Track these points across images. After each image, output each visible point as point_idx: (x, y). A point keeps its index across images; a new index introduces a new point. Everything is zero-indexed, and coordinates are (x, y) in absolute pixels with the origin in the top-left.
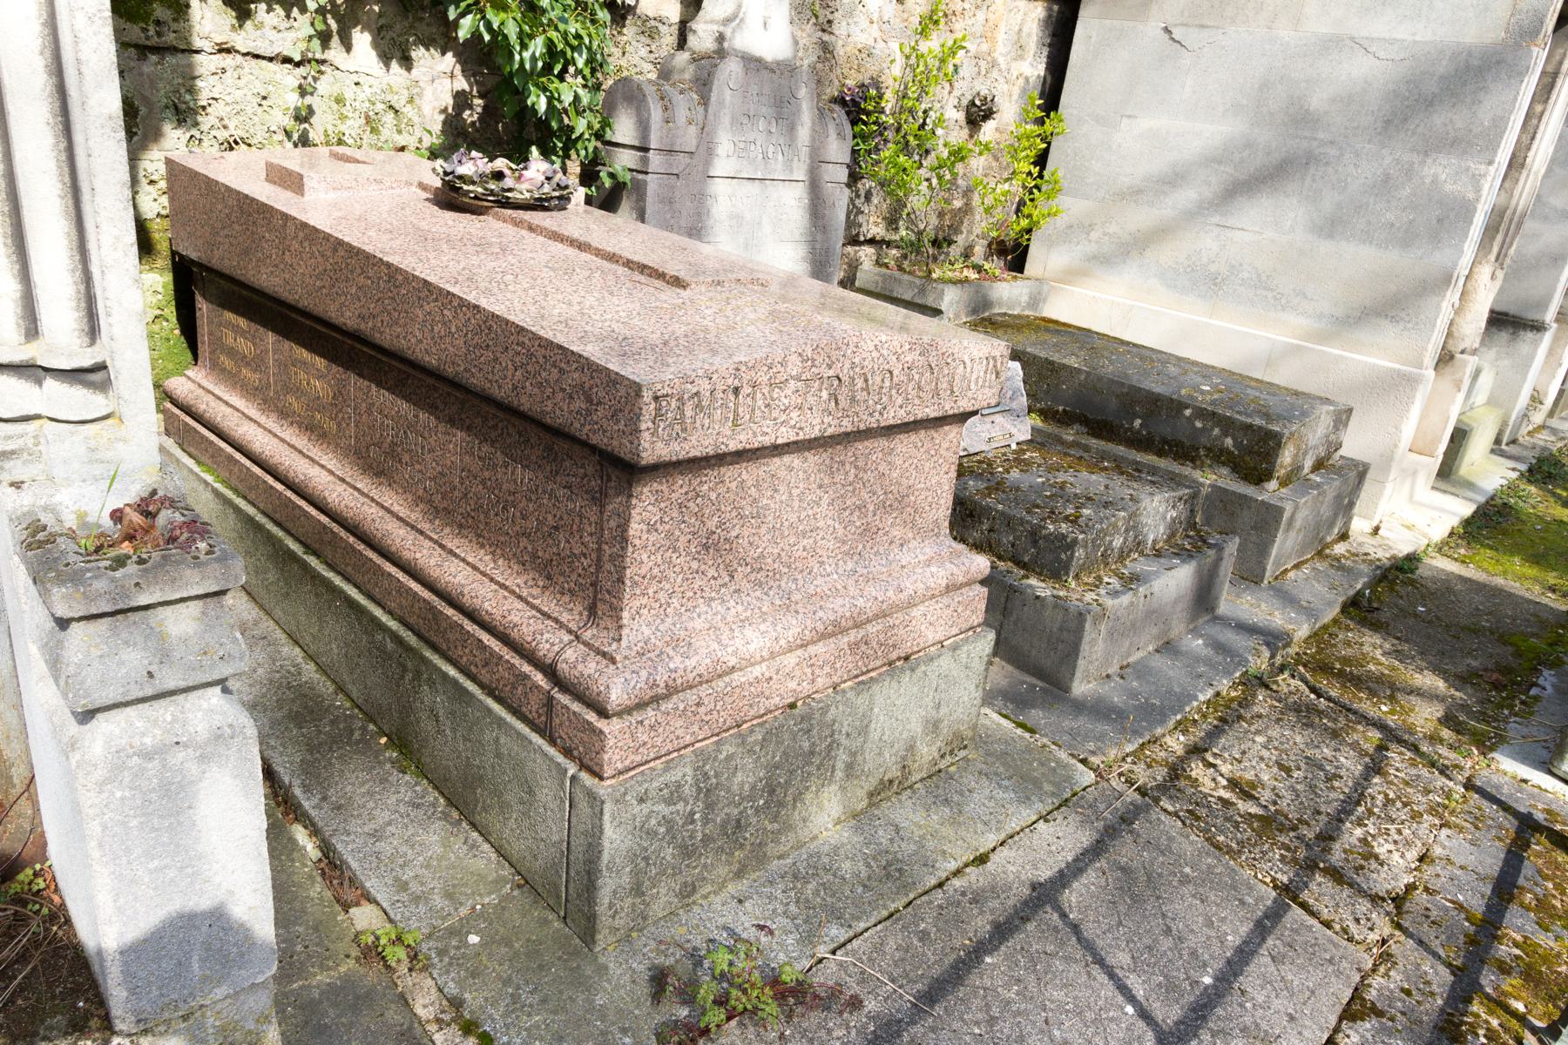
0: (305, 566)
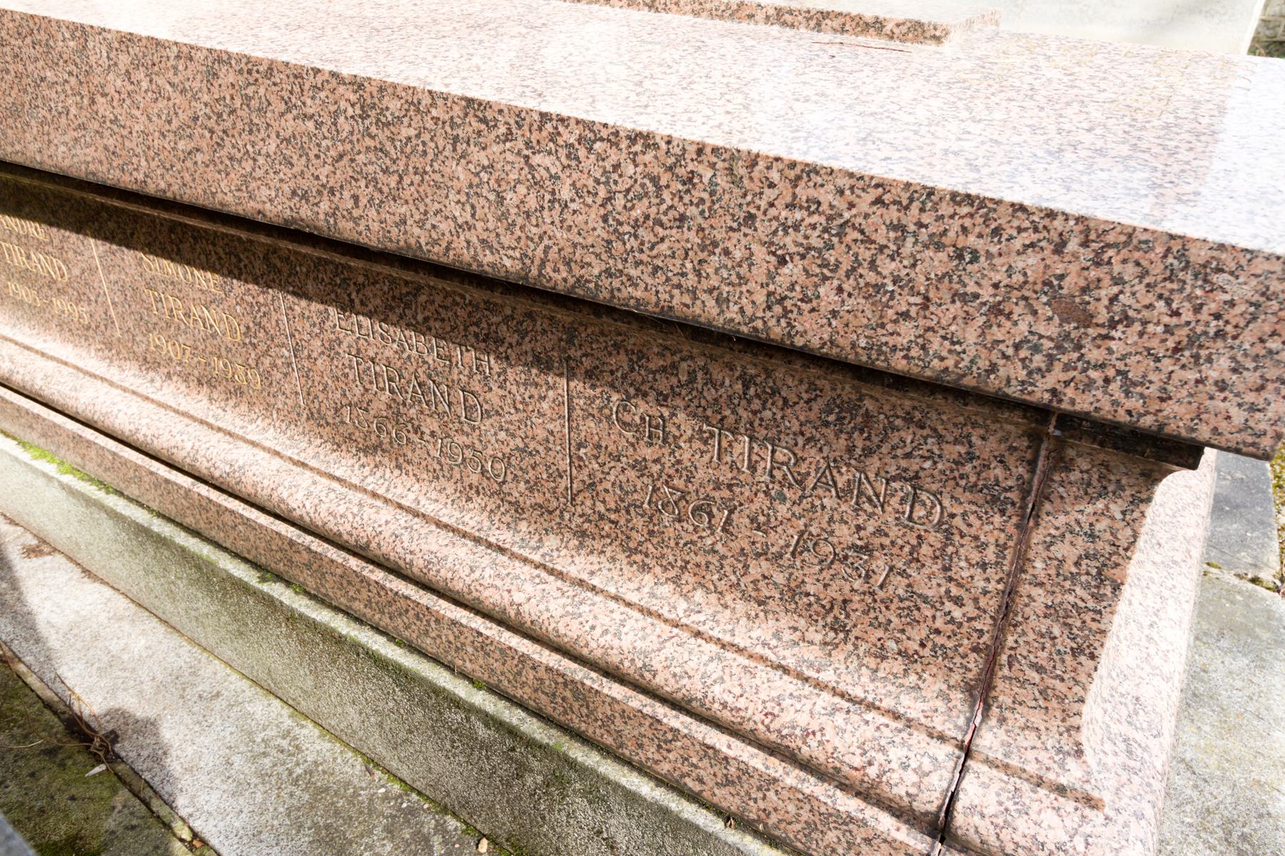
0: (270, 603)
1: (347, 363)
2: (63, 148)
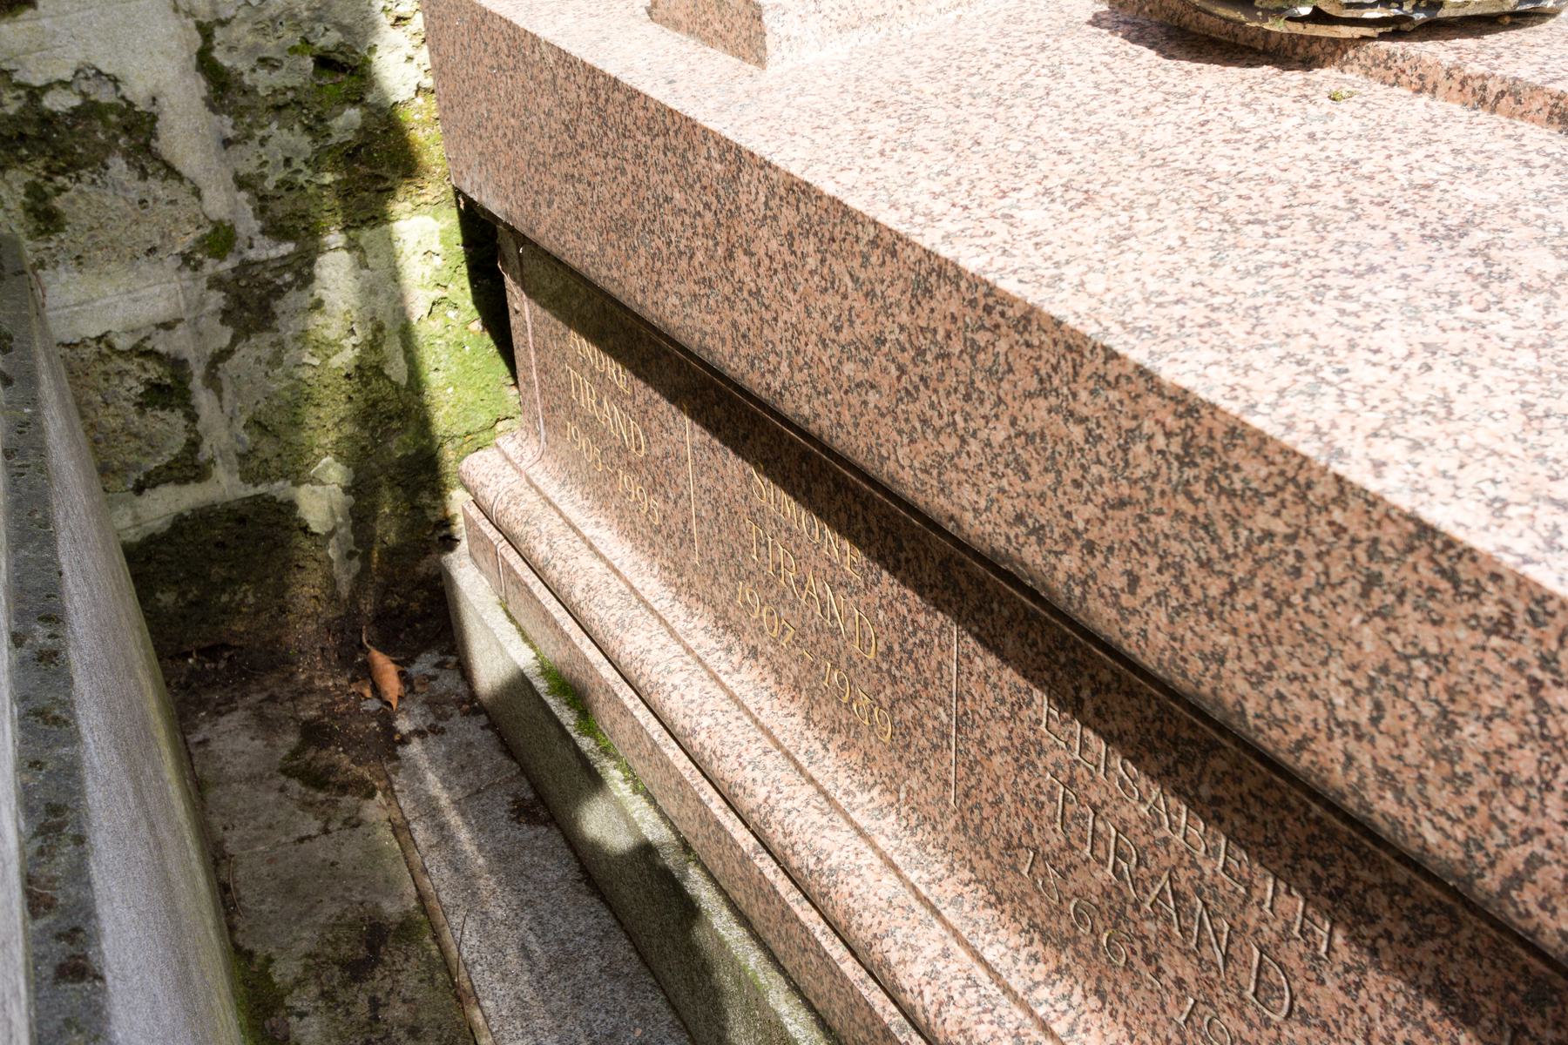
1: (1046, 788)
2: (674, 300)
